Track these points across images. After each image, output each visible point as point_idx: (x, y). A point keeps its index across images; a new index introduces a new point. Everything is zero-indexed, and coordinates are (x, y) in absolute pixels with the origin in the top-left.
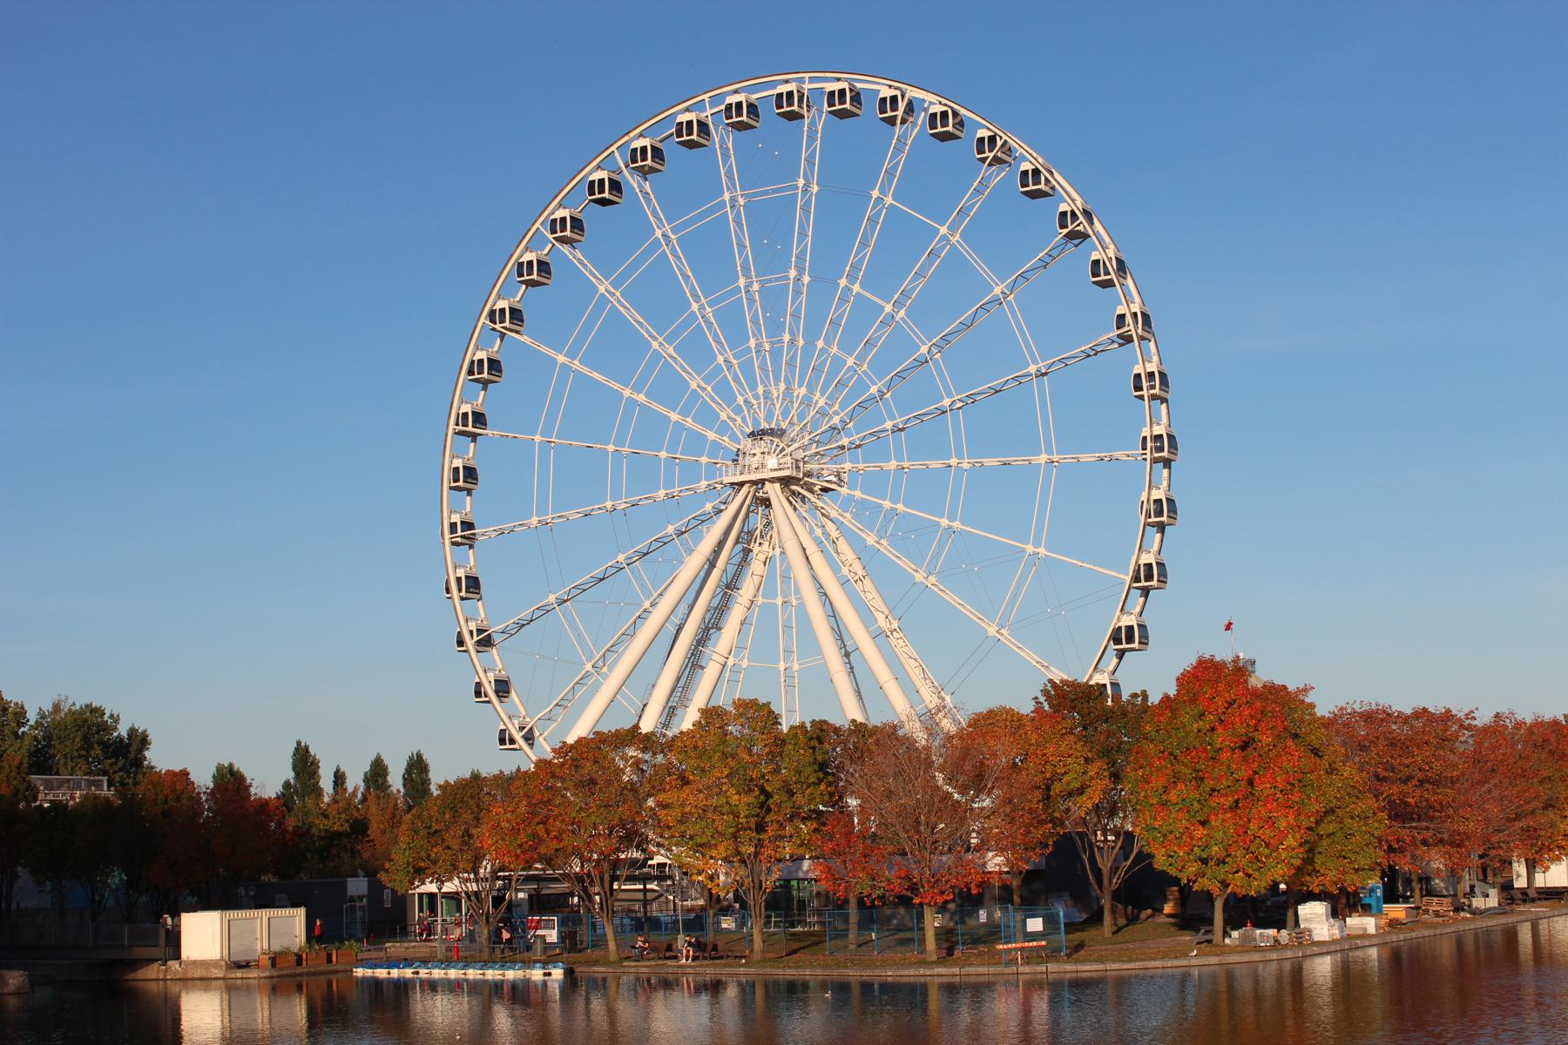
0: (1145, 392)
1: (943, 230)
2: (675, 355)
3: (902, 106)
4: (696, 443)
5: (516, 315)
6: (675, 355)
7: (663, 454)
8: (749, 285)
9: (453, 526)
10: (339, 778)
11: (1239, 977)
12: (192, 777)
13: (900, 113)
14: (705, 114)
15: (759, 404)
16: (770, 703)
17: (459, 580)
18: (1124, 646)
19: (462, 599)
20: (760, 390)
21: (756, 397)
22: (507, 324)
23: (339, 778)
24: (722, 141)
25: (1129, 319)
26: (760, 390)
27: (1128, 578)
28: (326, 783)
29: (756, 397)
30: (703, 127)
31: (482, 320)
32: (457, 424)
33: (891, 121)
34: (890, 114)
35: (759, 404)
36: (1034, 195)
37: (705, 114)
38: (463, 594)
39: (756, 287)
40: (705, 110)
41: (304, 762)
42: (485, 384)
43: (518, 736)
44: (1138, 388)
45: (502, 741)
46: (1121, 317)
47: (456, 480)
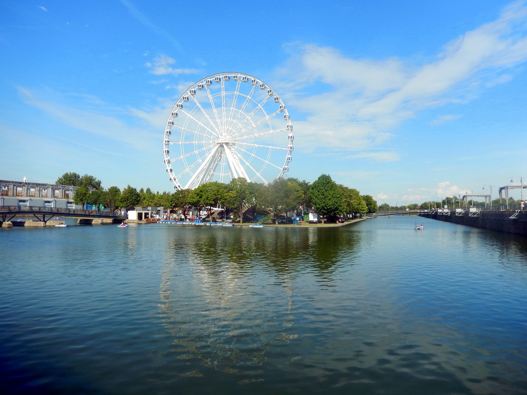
0: (290, 139)
1: (235, 121)
2: (216, 113)
3: (256, 82)
4: (211, 134)
5: (182, 106)
6: (216, 113)
7: (205, 135)
8: (224, 108)
9: (166, 141)
10: (160, 194)
11: (233, 332)
12: (102, 185)
13: (255, 83)
14: (203, 83)
15: (223, 129)
16: (217, 181)
17: (166, 151)
18: (285, 171)
19: (166, 154)
20: (224, 127)
21: (223, 128)
22: (180, 107)
23: (160, 194)
24: (223, 82)
25: (289, 126)
26: (224, 127)
27: (282, 169)
28: (159, 194)
29: (223, 128)
30: (220, 79)
31: (176, 106)
32: (169, 123)
33: (253, 84)
34: (253, 83)
35: (223, 129)
36: (276, 102)
37: (203, 83)
38: (166, 153)
39: (225, 109)
40: (203, 83)
41: (158, 193)
42: (174, 117)
43: (173, 179)
44: (289, 138)
45: (170, 180)
46: (288, 126)
47: (167, 133)
